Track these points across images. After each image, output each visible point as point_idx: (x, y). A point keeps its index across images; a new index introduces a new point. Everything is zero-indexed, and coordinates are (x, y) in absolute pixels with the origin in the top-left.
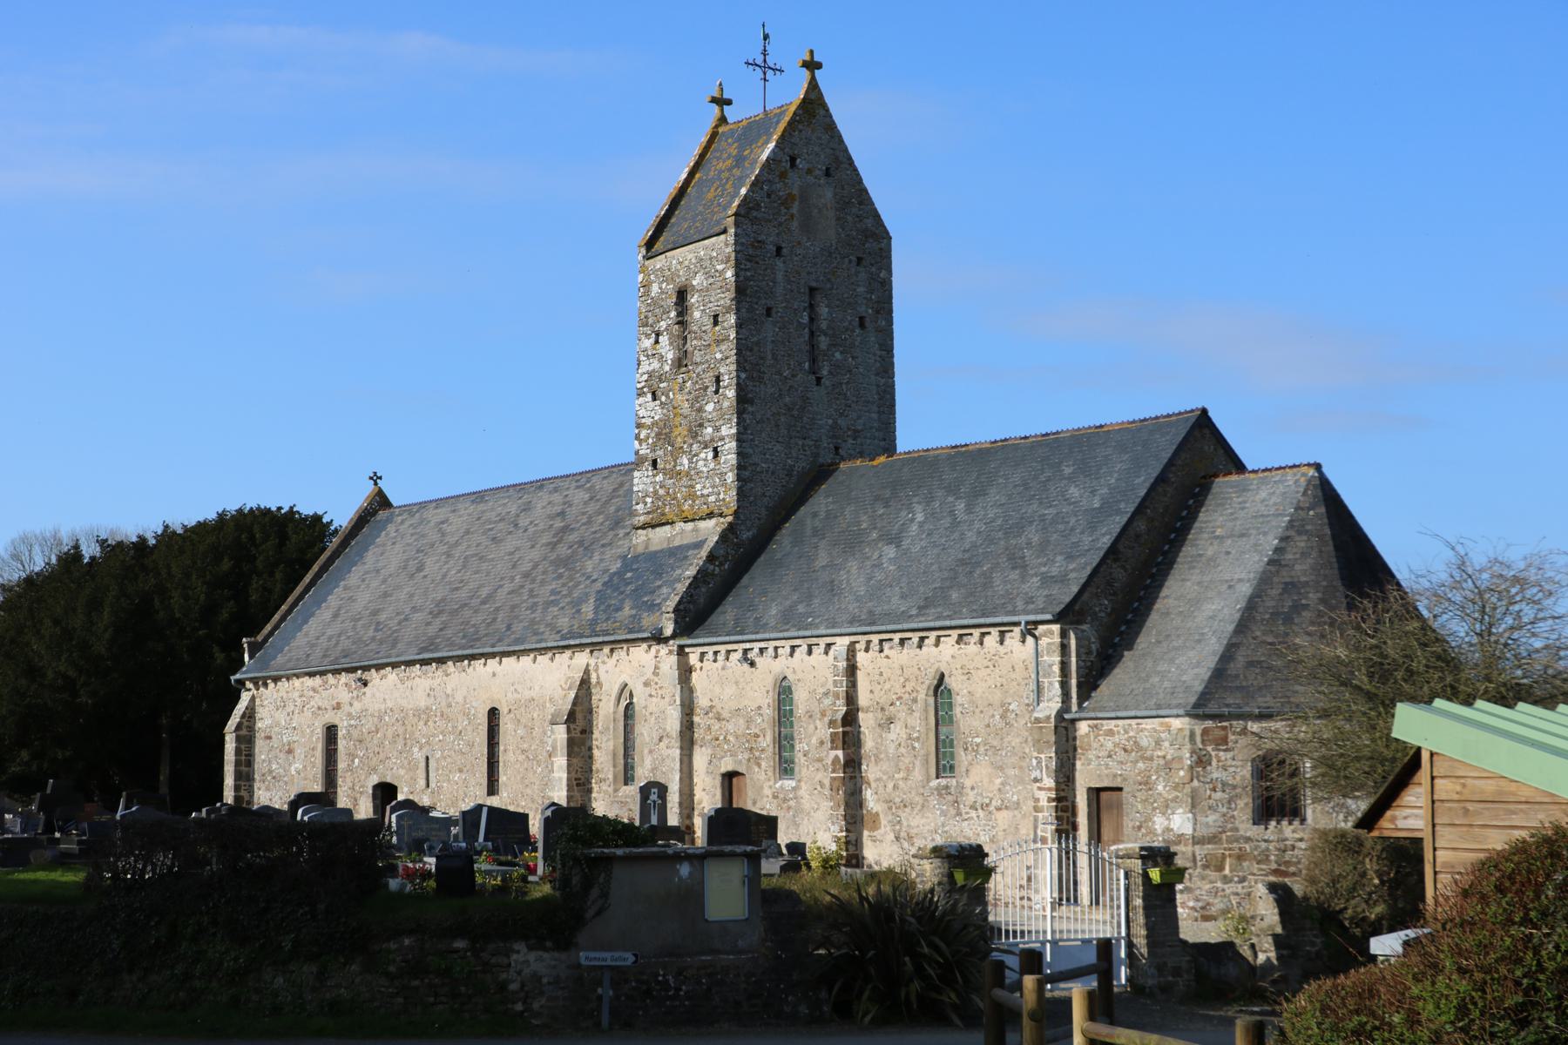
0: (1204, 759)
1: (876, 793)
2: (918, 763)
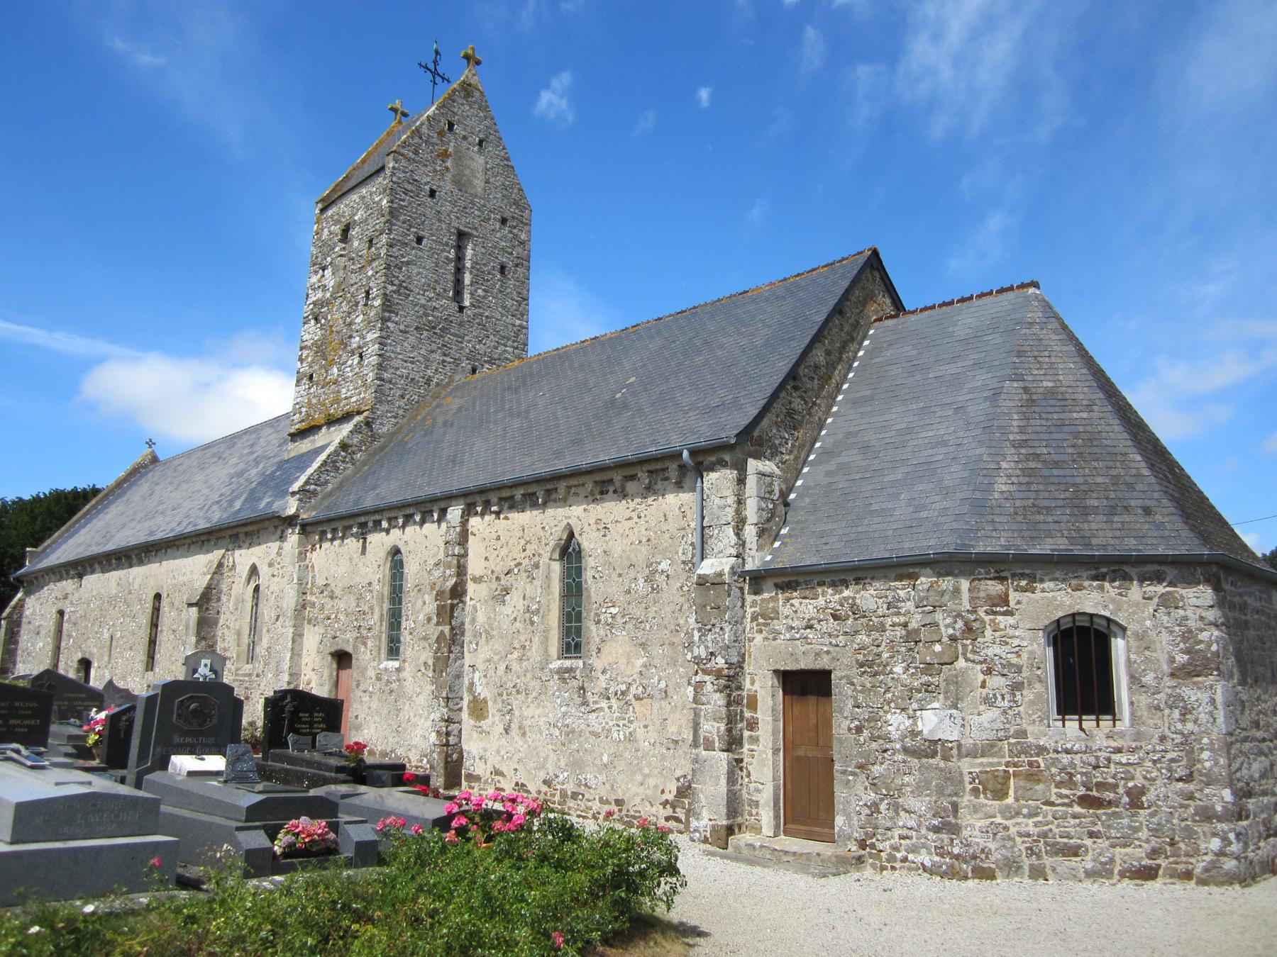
0: (975, 625)
1: (485, 676)
2: (536, 640)
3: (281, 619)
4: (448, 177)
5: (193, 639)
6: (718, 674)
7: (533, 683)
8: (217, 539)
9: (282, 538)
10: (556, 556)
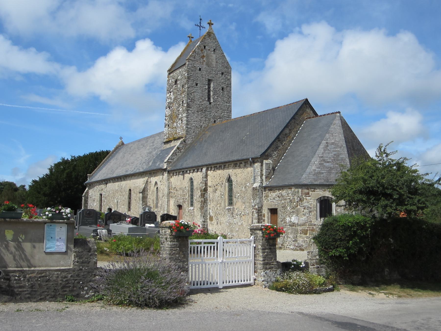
0: (302, 199)
3: (164, 196)
4: (205, 63)
5: (141, 202)
6: (256, 209)
7: (222, 212)
8: (146, 174)
9: (163, 175)
10: (227, 181)
